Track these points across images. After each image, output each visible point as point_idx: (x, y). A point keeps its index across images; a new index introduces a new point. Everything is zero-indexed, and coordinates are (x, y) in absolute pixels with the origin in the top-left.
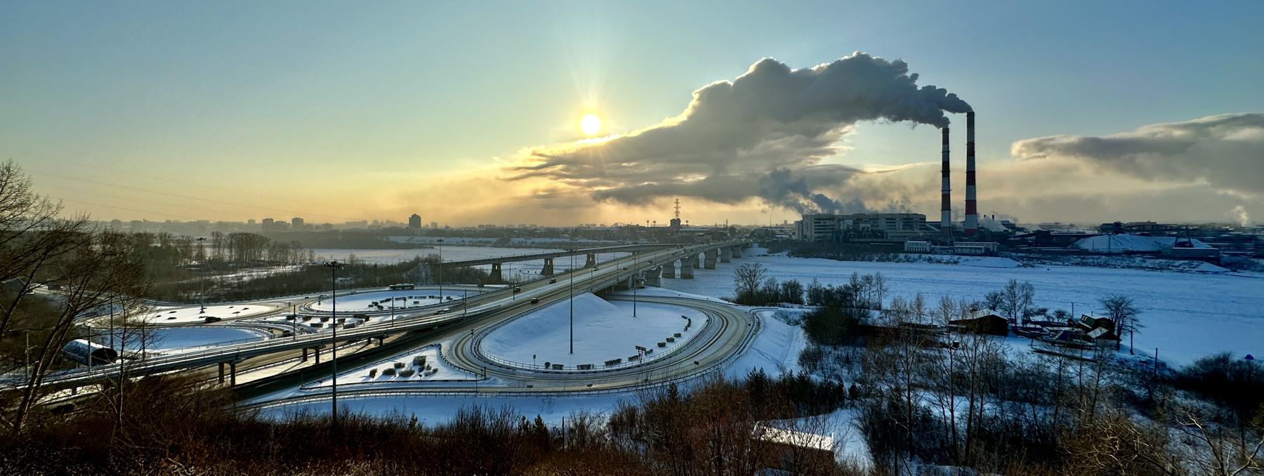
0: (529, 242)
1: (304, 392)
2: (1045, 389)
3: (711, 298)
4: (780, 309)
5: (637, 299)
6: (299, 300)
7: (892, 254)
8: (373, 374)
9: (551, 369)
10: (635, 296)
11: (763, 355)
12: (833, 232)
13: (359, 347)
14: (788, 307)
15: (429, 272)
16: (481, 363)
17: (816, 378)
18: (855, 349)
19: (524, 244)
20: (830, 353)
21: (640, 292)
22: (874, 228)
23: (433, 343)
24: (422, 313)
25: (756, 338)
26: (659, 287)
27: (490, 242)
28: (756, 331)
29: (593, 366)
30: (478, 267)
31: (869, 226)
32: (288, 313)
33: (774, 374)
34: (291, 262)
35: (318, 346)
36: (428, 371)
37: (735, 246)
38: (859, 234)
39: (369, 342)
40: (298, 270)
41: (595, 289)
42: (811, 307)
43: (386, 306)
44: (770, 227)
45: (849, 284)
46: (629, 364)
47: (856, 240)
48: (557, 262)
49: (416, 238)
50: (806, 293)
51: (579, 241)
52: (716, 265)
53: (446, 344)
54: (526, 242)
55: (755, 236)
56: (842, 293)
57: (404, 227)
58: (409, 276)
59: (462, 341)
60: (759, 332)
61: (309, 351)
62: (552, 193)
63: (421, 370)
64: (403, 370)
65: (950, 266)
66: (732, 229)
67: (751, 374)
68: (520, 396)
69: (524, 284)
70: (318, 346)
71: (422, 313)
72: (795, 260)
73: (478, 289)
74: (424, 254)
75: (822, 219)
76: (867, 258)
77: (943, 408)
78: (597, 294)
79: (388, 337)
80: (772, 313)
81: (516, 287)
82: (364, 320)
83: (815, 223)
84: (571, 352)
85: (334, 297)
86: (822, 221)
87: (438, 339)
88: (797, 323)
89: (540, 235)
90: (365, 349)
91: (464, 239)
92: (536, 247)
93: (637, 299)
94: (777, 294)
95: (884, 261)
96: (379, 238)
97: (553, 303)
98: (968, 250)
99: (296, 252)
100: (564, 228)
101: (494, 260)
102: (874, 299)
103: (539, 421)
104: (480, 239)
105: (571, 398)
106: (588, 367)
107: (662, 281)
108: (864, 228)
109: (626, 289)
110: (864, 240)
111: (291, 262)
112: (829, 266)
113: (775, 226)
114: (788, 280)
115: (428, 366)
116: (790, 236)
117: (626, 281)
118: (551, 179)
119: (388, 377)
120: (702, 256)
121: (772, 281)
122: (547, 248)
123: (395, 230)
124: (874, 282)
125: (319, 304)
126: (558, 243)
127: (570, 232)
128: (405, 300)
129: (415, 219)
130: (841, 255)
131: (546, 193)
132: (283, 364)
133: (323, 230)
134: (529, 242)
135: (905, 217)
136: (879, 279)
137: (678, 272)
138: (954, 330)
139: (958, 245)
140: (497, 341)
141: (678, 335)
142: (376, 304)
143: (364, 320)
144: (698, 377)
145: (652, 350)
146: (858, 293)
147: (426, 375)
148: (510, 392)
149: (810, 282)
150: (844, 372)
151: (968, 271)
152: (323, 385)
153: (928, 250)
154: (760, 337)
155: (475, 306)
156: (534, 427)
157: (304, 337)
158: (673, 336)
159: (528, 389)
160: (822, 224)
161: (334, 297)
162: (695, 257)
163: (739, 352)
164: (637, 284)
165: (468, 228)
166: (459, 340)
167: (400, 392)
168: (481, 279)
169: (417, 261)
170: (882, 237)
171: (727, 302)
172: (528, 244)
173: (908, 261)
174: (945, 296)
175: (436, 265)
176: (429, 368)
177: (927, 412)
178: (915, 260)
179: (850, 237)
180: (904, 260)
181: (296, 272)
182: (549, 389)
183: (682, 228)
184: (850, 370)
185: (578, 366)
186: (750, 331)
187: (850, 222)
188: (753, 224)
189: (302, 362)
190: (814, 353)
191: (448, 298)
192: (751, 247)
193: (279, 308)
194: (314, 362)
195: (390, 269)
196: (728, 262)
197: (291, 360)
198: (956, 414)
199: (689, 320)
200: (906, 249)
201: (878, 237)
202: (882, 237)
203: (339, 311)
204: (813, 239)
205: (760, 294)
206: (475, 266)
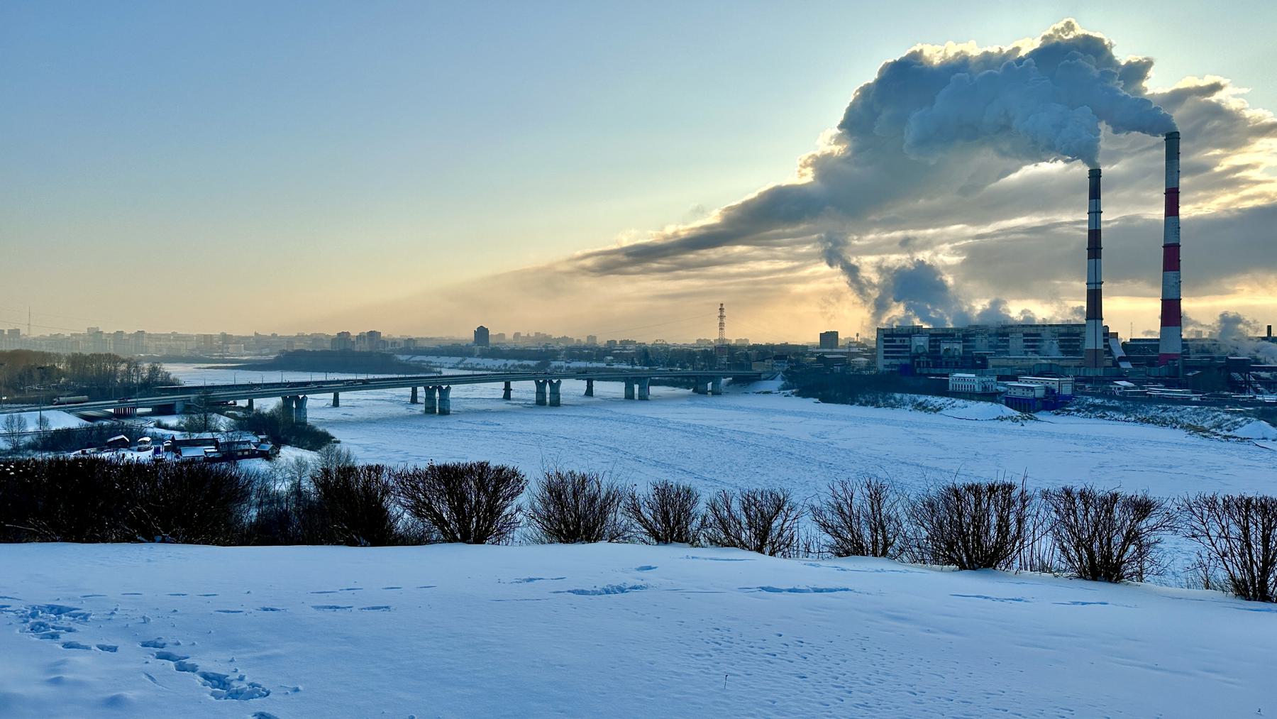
2: (628, 475)
75: (898, 335)
83: (885, 341)
86: (898, 339)
108: (947, 350)
129: (482, 333)
131: (1241, 186)
135: (1063, 330)
160: (898, 343)
203: (597, 393)
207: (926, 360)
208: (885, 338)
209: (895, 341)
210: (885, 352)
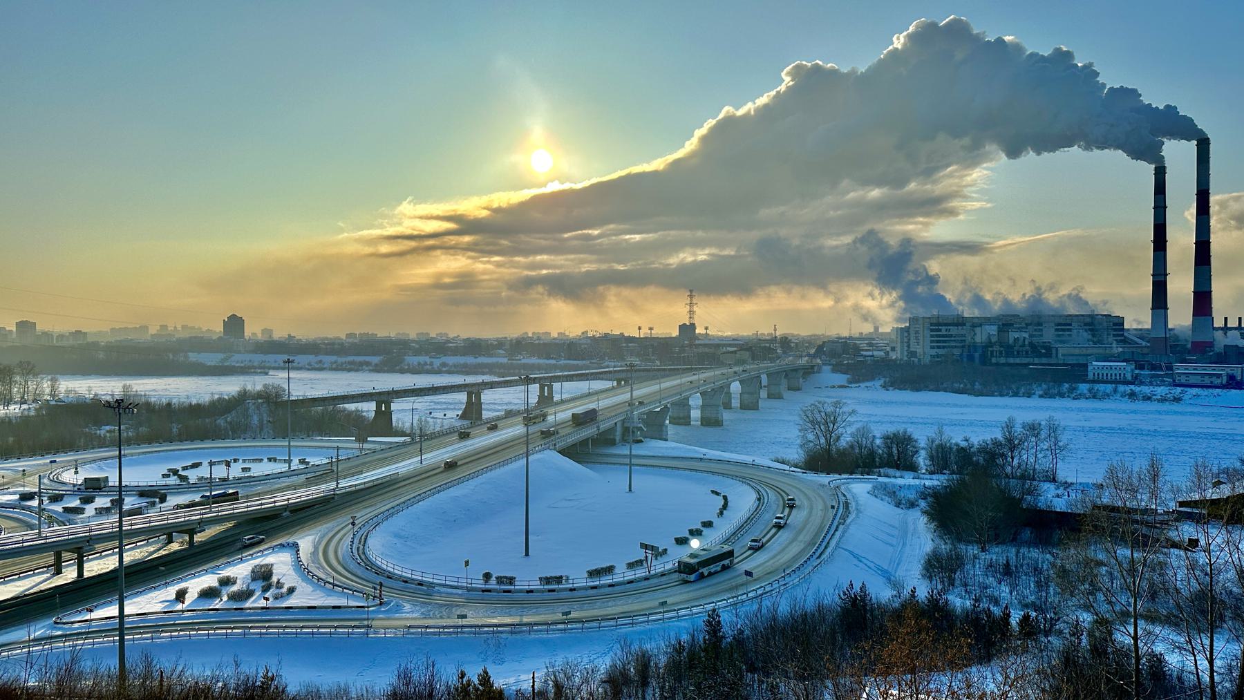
0: (437, 363)
1: (60, 629)
3: (759, 461)
4: (881, 479)
5: (634, 461)
6: (40, 465)
7: (1067, 385)
8: (181, 596)
9: (493, 584)
10: (631, 456)
11: (861, 561)
12: (963, 347)
13: (152, 549)
14: (895, 477)
15: (265, 415)
16: (373, 577)
17: (958, 601)
18: (1018, 552)
19: (428, 367)
20: (975, 557)
21: (638, 450)
22: (1035, 340)
23: (282, 541)
24: (259, 489)
25: (845, 531)
26: (667, 440)
27: (368, 364)
28: (844, 518)
29: (568, 578)
30: (351, 407)
31: (1026, 335)
32: (22, 489)
33: (882, 594)
34: (17, 398)
35: (81, 548)
36: (277, 591)
37: (793, 370)
38: (1009, 350)
39: (170, 541)
40: (32, 413)
41: (561, 444)
42: (934, 476)
43: (193, 475)
44: (851, 338)
45: (1000, 437)
46: (630, 575)
47: (1002, 360)
48: (487, 396)
49: (237, 357)
50: (923, 453)
51: (523, 361)
52: (761, 404)
53: (306, 542)
54: (431, 364)
55: (824, 353)
56: (987, 453)
57: (215, 337)
58: (230, 423)
59: (339, 531)
60: (848, 521)
61: (65, 555)
62: (465, 280)
63: (266, 589)
64: (234, 588)
65: (1166, 406)
66: (785, 342)
67: (845, 594)
68: (445, 633)
69: (434, 436)
70: (81, 549)
71: (259, 489)
72: (895, 395)
73: (357, 445)
74: (255, 384)
76: (1023, 390)
77: (1195, 656)
78: (563, 452)
79: (204, 530)
80: (869, 486)
81: (421, 438)
82: (158, 500)
83: (932, 330)
84: (527, 554)
85: (120, 457)
86: (943, 328)
87: (292, 534)
88: (912, 505)
89: (456, 351)
90: (163, 552)
91: (320, 357)
92: (449, 372)
93: (634, 461)
94: (872, 454)
95: (1052, 396)
96: (171, 356)
97: (490, 469)
98: (1199, 377)
99: (26, 382)
100: (497, 340)
101: (380, 393)
102: (1044, 463)
103: (485, 679)
104: (350, 358)
105: (533, 636)
106: (559, 580)
107: (671, 430)
108: (1016, 340)
109: (612, 443)
110: (1018, 361)
111: (17, 398)
112: (956, 405)
113: (858, 335)
114: (891, 429)
115: (278, 582)
116: (887, 353)
117: (612, 430)
118: (469, 257)
119: (210, 601)
120: (736, 387)
121: (864, 432)
122: (468, 373)
123: (200, 343)
124: (1043, 435)
125: (76, 473)
126: (488, 364)
127: (507, 347)
128: (228, 464)
129: (234, 324)
130: (977, 386)
132: (19, 579)
133: (71, 342)
134: (437, 363)
136: (1054, 429)
137: (695, 414)
138: (1189, 517)
139: (1180, 369)
140: (397, 536)
141: (708, 524)
142: (175, 472)
143: (158, 500)
144: (753, 598)
145: (666, 550)
146: (1016, 453)
147: (276, 598)
148: (427, 627)
149: (931, 432)
150: (1004, 591)
151: (1200, 414)
152: (95, 615)
153: (1129, 377)
154: (852, 529)
155: (353, 474)
156: (477, 689)
157: (55, 532)
158: (699, 526)
159: (460, 622)
161: (120, 457)
162: (724, 389)
163: (818, 554)
164: (630, 434)
165: (327, 339)
166: (330, 535)
167: (215, 629)
168: (360, 428)
169: (243, 396)
170: (1048, 355)
171: (787, 468)
172: (435, 366)
173: (1094, 397)
174: (1200, 461)
175: (276, 403)
176: (279, 585)
177: (1158, 660)
178: (1106, 396)
179: (992, 355)
180: (1088, 395)
181: (28, 417)
182: (495, 621)
183: (699, 339)
184: (1013, 587)
185: (541, 579)
186: (834, 519)
187: (993, 330)
188: (819, 332)
189: (54, 575)
190: (950, 558)
191: (302, 461)
192: (819, 371)
193: (5, 480)
194: (75, 574)
195: (195, 410)
196: (780, 397)
197: (33, 571)
198: (1218, 663)
199: (725, 498)
200: (1090, 376)
201: (1041, 355)
202: (1048, 355)
203: (128, 484)
204: (927, 360)
205: (843, 453)
206: (347, 406)
207: (998, 349)
208: (931, 327)
209: (940, 330)
210: (932, 341)
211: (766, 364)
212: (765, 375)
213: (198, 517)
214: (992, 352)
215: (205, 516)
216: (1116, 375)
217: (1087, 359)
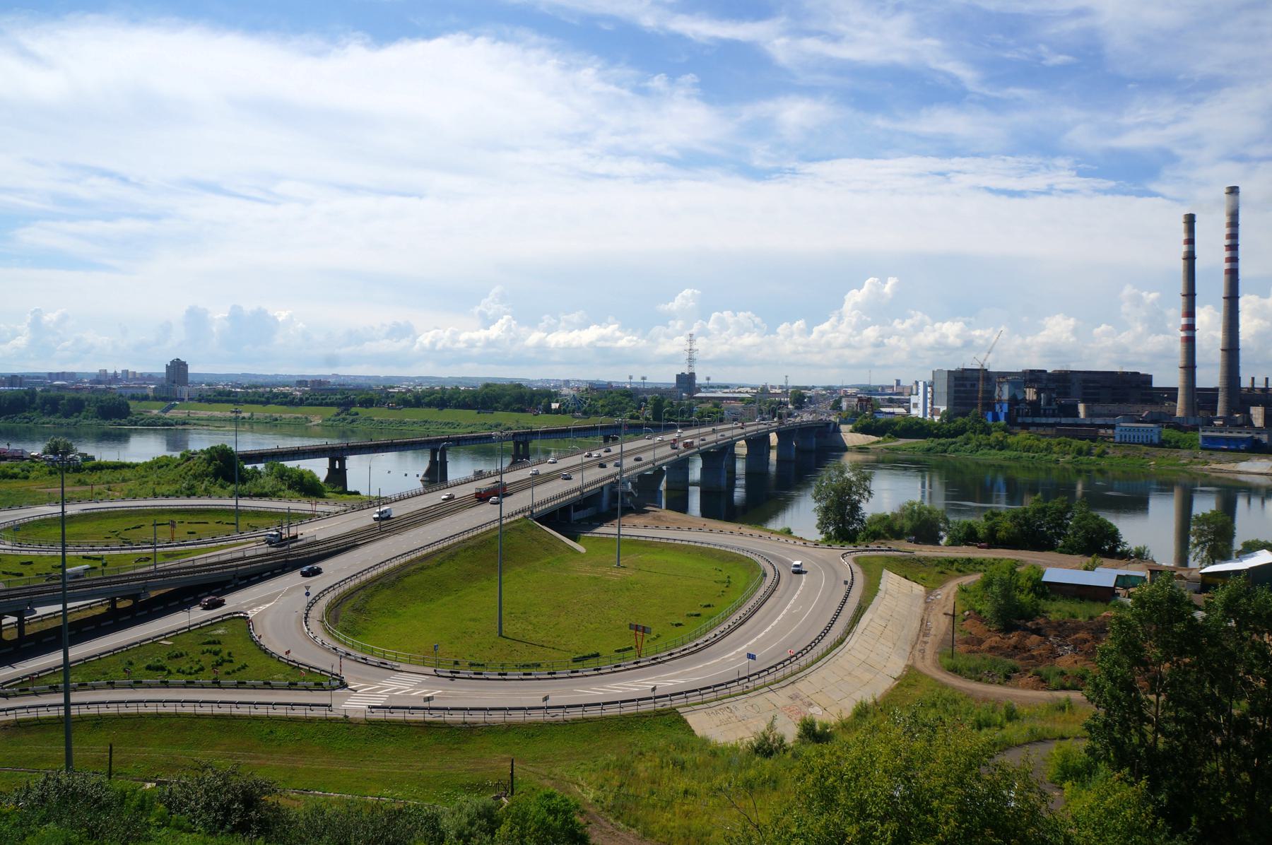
30: (290, 464)
211: (775, 423)
212: (774, 433)
213: (234, 569)
214: (1018, 410)
215: (239, 568)
216: (1143, 437)
217: (1115, 420)
